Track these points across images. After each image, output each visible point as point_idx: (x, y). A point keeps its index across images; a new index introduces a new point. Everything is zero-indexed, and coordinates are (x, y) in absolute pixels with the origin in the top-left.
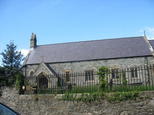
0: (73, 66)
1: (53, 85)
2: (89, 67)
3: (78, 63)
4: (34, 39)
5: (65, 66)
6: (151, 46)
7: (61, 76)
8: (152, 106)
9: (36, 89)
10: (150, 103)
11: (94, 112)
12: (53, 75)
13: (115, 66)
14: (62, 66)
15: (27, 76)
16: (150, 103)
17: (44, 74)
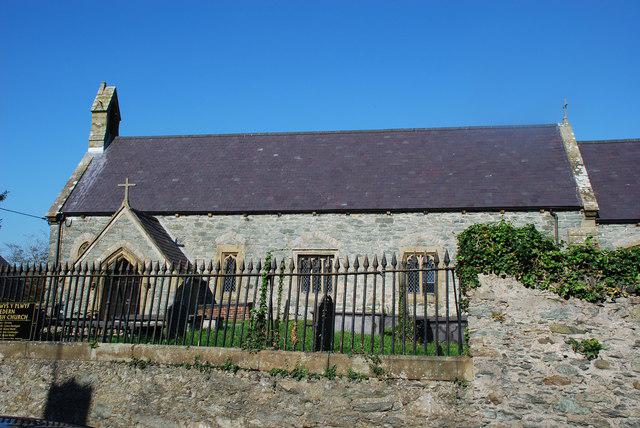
0: (254, 230)
1: (155, 305)
2: (317, 240)
3: (274, 218)
4: (106, 109)
5: (220, 227)
6: (584, 169)
7: (206, 272)
8: (424, 414)
9: (26, 317)
10: (418, 404)
11: (220, 421)
12: (168, 266)
13: (420, 242)
14: (210, 227)
15: (63, 261)
16: (418, 404)
17: (129, 259)
